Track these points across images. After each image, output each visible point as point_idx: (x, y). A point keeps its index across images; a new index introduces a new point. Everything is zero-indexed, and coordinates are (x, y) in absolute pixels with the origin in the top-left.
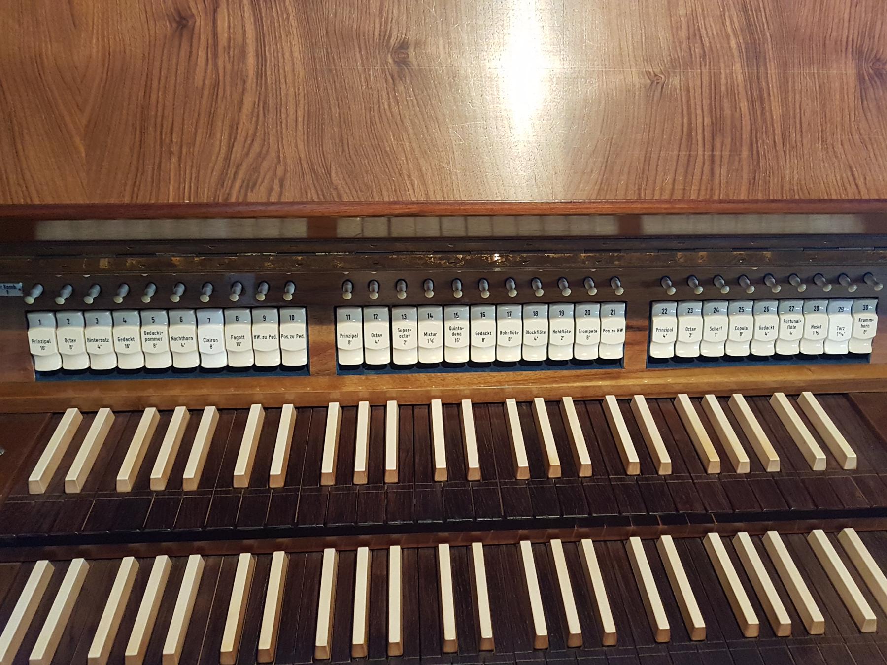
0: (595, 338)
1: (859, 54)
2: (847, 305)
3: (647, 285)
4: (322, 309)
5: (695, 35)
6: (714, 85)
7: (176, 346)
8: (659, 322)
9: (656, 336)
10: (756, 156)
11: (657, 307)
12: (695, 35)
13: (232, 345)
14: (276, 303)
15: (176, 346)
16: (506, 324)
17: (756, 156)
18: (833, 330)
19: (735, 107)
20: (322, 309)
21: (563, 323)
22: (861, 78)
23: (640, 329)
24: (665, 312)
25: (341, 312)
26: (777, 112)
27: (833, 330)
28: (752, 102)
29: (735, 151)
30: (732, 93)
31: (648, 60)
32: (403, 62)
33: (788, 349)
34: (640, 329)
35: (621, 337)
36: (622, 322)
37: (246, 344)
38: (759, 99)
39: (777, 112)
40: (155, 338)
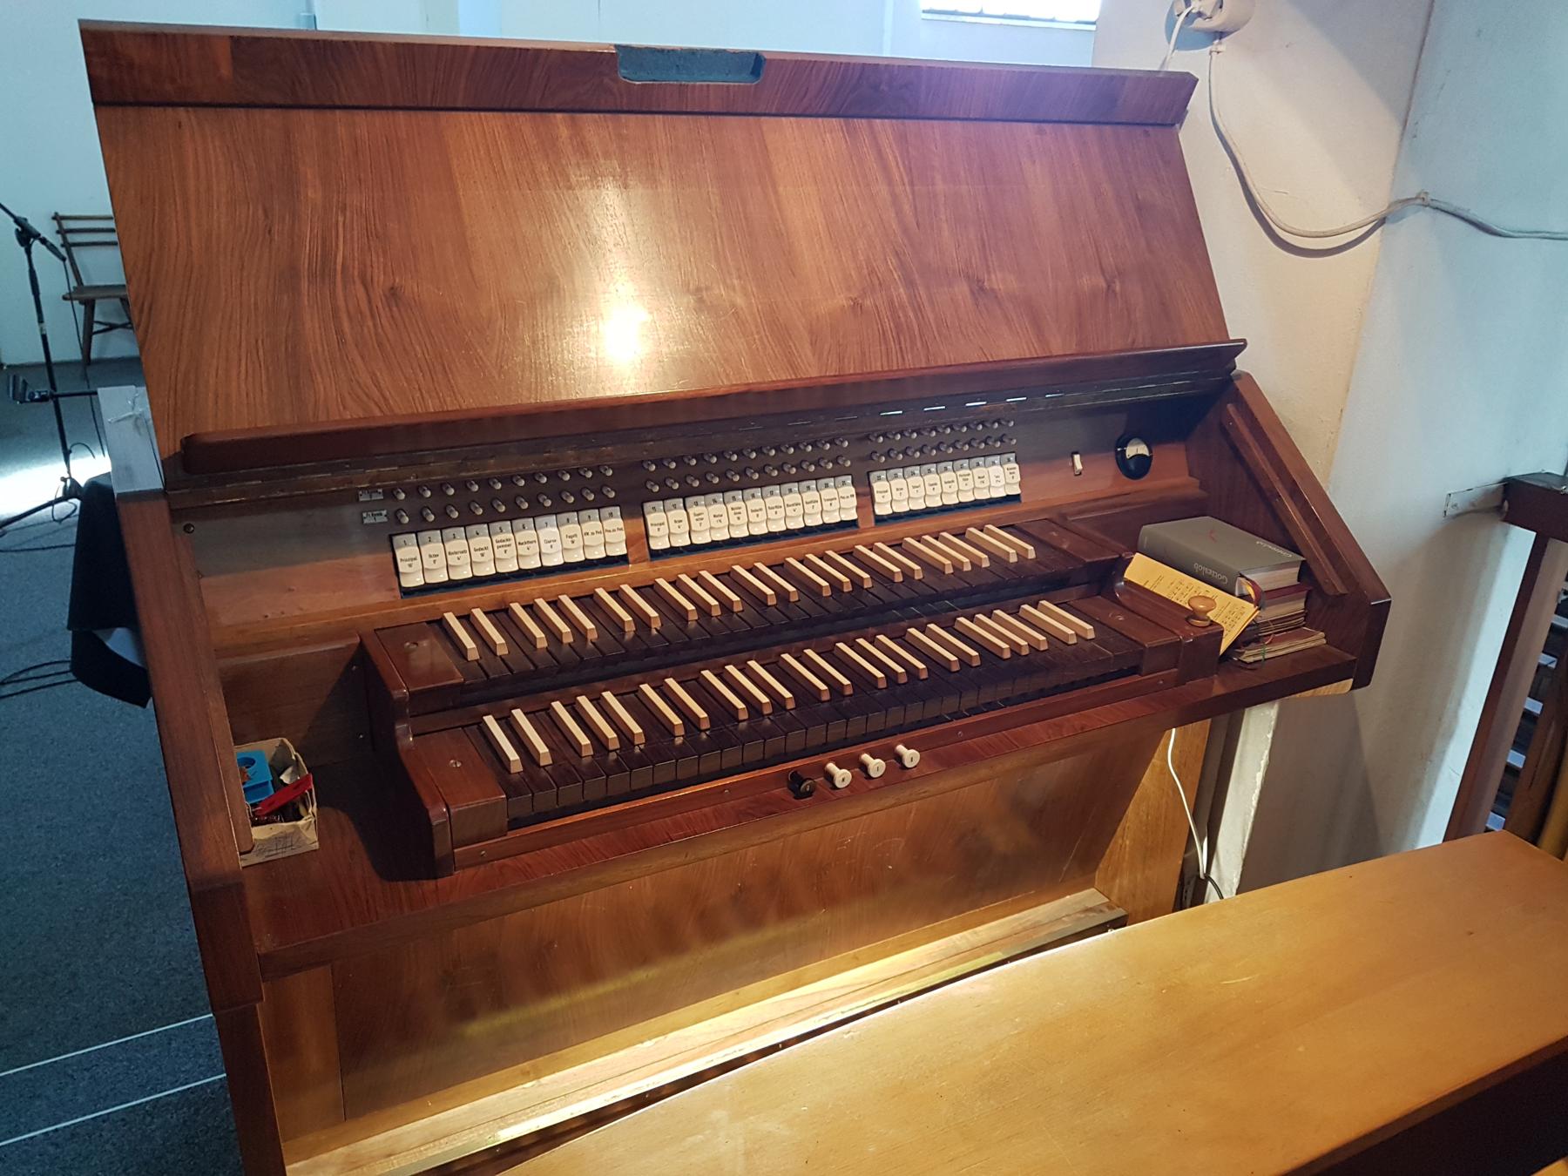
0: (762, 515)
1: (968, 277)
2: (997, 459)
3: (862, 459)
4: (633, 508)
5: (872, 272)
6: (891, 302)
7: (522, 550)
8: (877, 486)
9: (878, 497)
10: (925, 345)
11: (873, 476)
12: (872, 272)
13: (568, 544)
14: (601, 504)
15: (522, 550)
16: (477, 542)
17: (925, 345)
18: (993, 479)
19: (906, 316)
20: (633, 508)
21: (458, 544)
22: (972, 293)
23: (866, 496)
24: (879, 479)
25: (648, 506)
26: (931, 317)
27: (993, 479)
28: (914, 310)
29: (913, 343)
30: (903, 307)
31: (849, 289)
32: (701, 300)
33: (967, 498)
34: (866, 496)
35: (854, 502)
36: (852, 490)
37: (579, 541)
38: (918, 309)
39: (931, 317)
40: (504, 544)
